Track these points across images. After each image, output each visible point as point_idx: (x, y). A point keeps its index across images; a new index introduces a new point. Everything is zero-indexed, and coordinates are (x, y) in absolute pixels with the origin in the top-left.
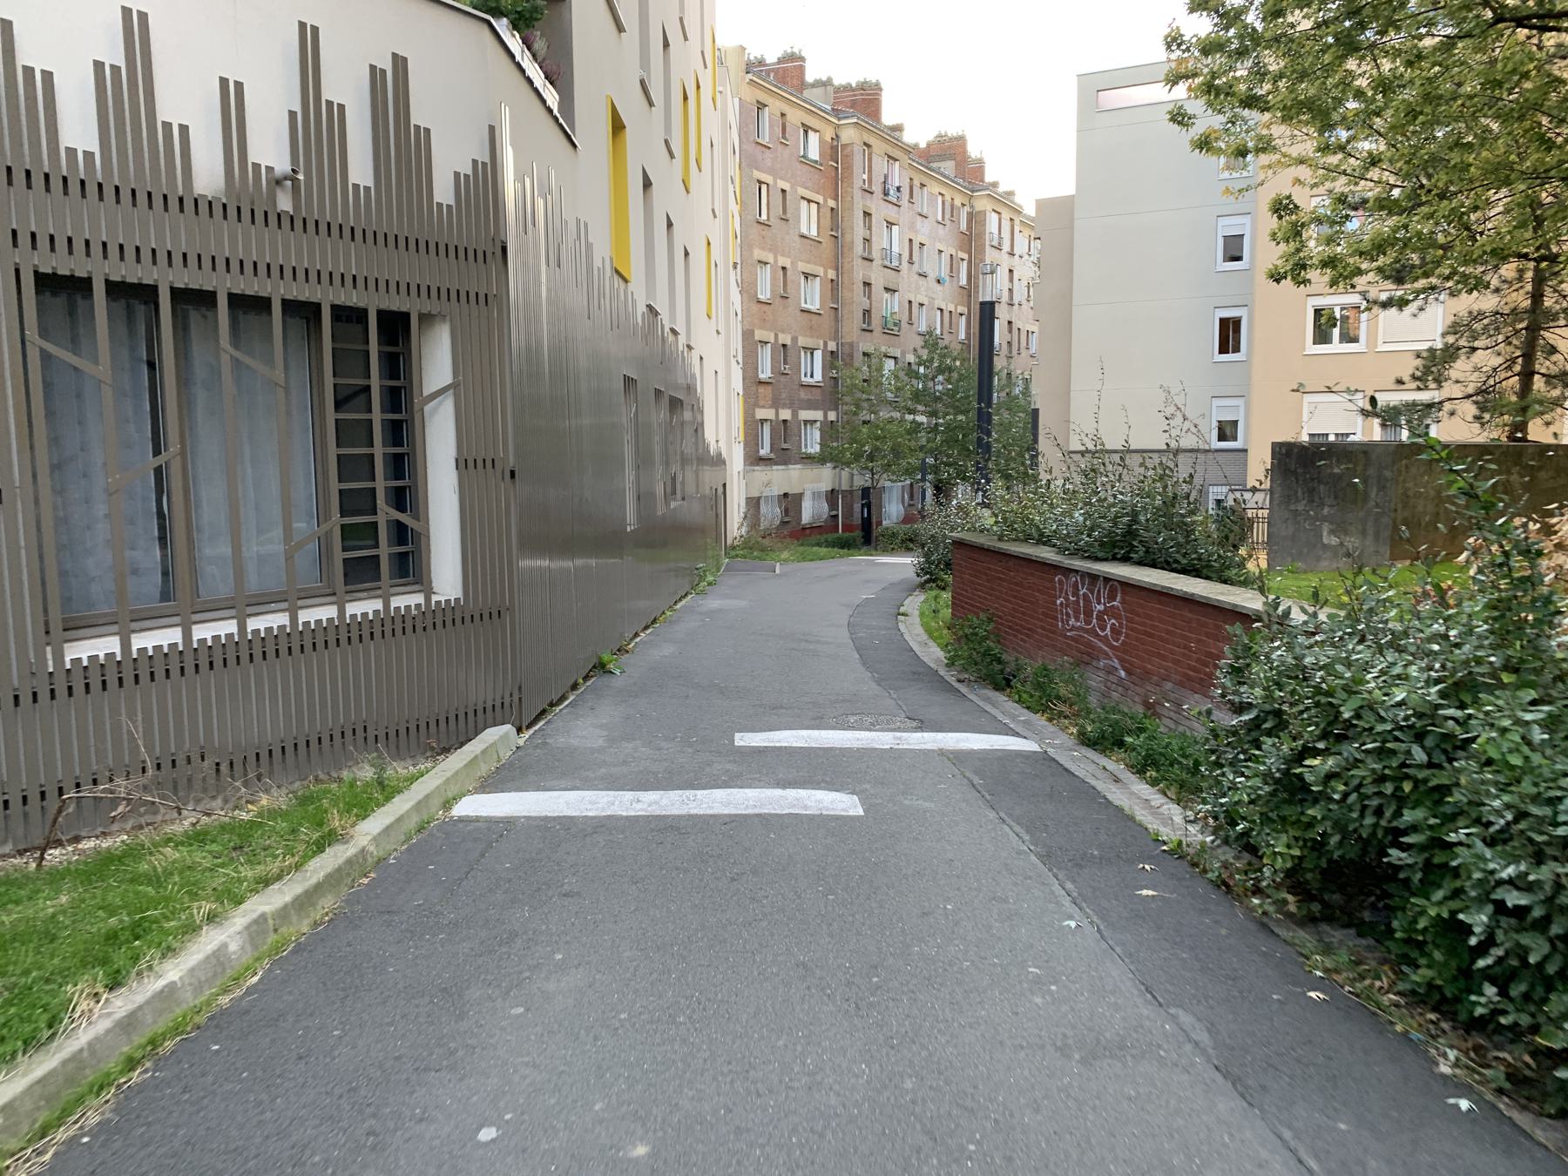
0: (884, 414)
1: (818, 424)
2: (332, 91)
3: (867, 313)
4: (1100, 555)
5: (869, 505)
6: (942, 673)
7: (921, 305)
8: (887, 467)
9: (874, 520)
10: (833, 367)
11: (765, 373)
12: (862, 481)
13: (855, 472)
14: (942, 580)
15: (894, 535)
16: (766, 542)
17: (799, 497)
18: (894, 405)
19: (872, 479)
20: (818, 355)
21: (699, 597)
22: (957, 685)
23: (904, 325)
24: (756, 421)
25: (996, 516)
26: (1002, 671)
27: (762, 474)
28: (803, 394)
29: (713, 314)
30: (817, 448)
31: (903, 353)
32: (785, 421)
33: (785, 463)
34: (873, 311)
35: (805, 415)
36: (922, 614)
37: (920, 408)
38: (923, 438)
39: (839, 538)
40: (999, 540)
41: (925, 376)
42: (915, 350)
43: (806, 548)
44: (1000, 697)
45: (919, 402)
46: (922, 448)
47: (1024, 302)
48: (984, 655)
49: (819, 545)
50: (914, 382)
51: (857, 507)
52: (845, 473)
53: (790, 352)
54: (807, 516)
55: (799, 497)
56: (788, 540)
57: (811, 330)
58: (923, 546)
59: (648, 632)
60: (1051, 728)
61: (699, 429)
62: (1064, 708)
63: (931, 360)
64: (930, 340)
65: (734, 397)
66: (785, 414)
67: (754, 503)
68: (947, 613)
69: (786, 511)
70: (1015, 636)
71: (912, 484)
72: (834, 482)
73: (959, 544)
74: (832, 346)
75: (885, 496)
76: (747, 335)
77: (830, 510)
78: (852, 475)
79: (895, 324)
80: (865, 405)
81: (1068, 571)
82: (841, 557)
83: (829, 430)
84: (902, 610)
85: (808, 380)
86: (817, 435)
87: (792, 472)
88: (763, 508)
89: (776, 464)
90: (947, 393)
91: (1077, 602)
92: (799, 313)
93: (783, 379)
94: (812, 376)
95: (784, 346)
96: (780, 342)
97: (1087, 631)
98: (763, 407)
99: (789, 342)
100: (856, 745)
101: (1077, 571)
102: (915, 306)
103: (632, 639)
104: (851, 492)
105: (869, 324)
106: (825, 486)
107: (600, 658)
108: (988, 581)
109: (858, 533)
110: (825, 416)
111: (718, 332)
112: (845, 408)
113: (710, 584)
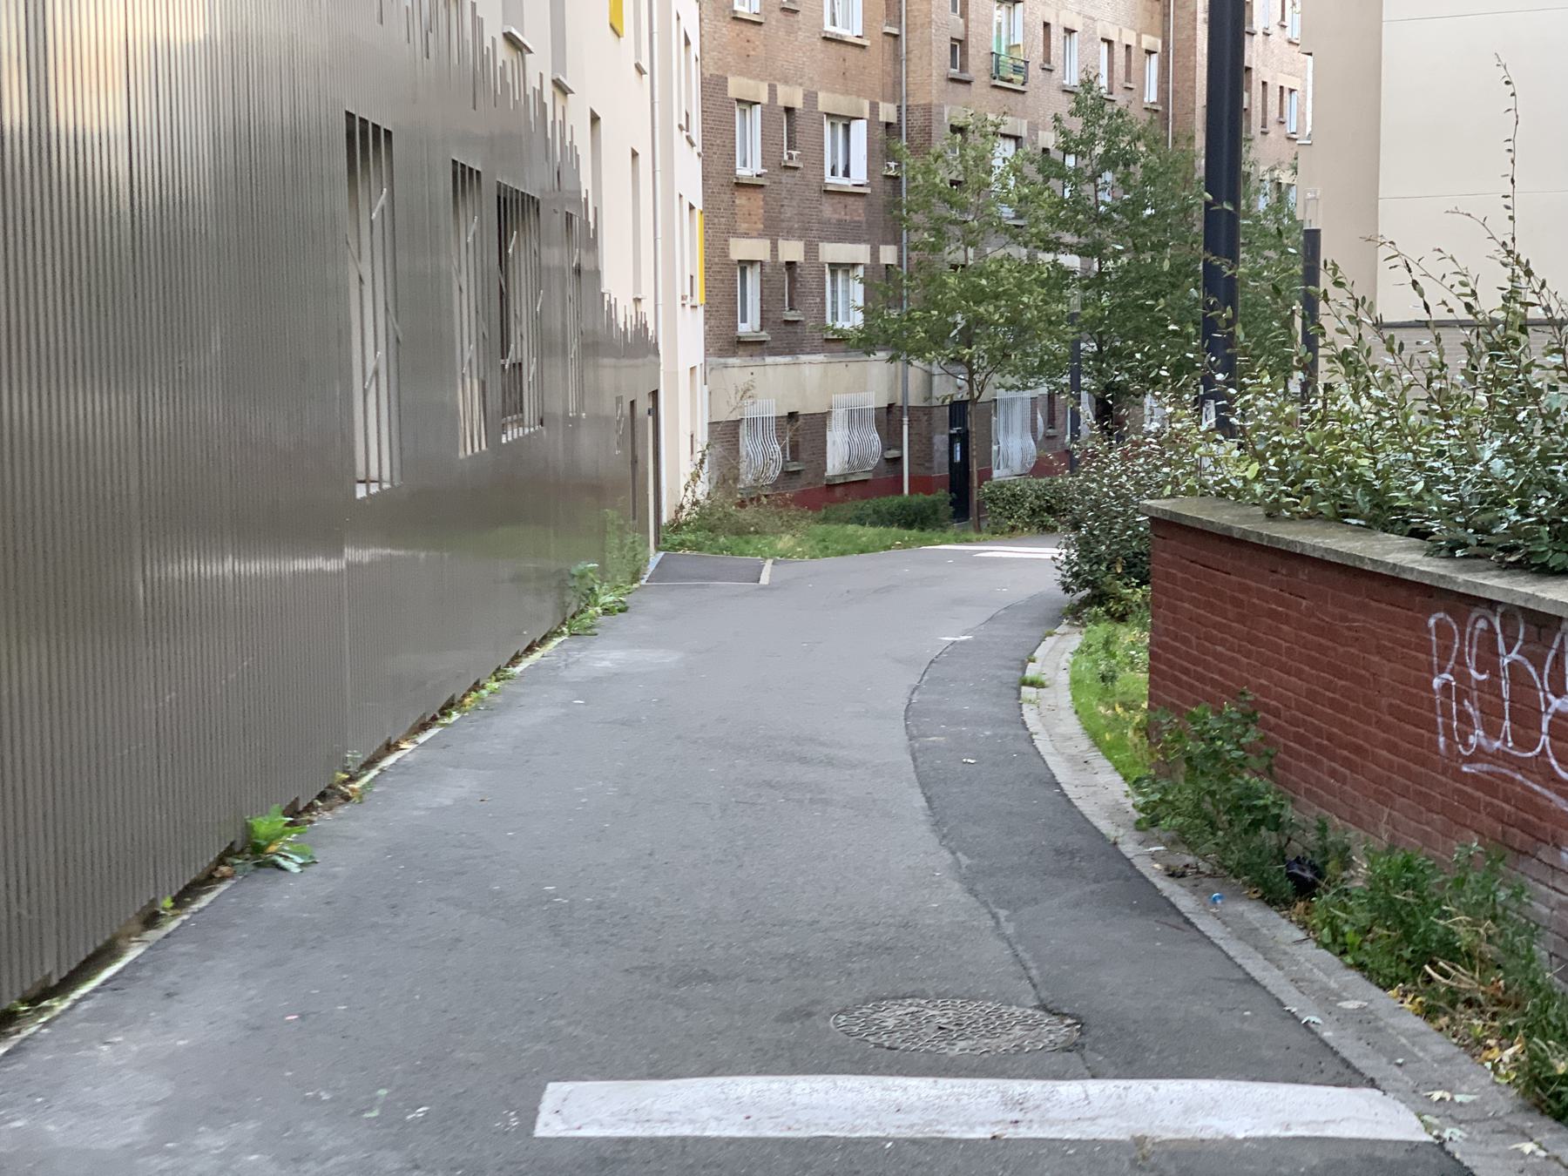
0: (995, 250)
1: (860, 271)
2: (545, 100)
3: (959, 46)
4: (1555, 560)
5: (964, 438)
6: (1129, 848)
7: (1070, 32)
8: (999, 359)
9: (974, 468)
10: (890, 154)
11: (750, 167)
12: (949, 387)
13: (936, 370)
14: (1119, 600)
15: (1016, 499)
16: (747, 515)
17: (819, 422)
18: (1014, 234)
19: (970, 382)
20: (859, 130)
21: (576, 644)
22: (1166, 886)
23: (1034, 70)
24: (729, 265)
25: (1263, 460)
26: (1280, 855)
27: (739, 370)
28: (829, 210)
29: (628, 28)
30: (858, 319)
31: (1034, 128)
32: (791, 265)
33: (792, 350)
34: (972, 40)
35: (833, 252)
36: (1076, 683)
37: (1068, 238)
38: (1074, 296)
39: (903, 507)
40: (1269, 516)
41: (1077, 171)
42: (1057, 119)
43: (833, 527)
44: (1283, 929)
45: (1063, 225)
46: (1072, 318)
47: (1274, 29)
48: (1235, 809)
49: (860, 521)
50: (1055, 183)
51: (940, 441)
52: (917, 369)
53: (800, 123)
54: (836, 461)
55: (819, 422)
56: (793, 511)
57: (845, 80)
58: (1076, 527)
59: (423, 738)
60: (1436, 1045)
61: (585, 276)
62: (1465, 981)
63: (1090, 141)
64: (1088, 101)
65: (680, 215)
66: (792, 250)
67: (726, 434)
68: (1136, 681)
69: (794, 451)
70: (1313, 762)
71: (1051, 397)
72: (892, 389)
73: (1165, 525)
74: (887, 112)
75: (998, 421)
76: (712, 87)
77: (886, 447)
78: (930, 375)
79: (1017, 70)
80: (956, 231)
81: (1464, 603)
82: (906, 545)
83: (882, 284)
84: (1032, 671)
85: (839, 181)
86: (858, 293)
87: (806, 369)
88: (746, 444)
89: (775, 352)
90: (1122, 208)
91: (1493, 686)
92: (819, 44)
93: (785, 177)
94: (847, 174)
95: (789, 111)
96: (781, 102)
97: (1520, 765)
98: (746, 235)
99: (798, 103)
100: (893, 1127)
101: (1492, 604)
102: (1057, 34)
103: (370, 764)
104: (928, 411)
105: (963, 68)
106: (875, 397)
107: (249, 829)
108: (1241, 619)
109: (942, 495)
110: (875, 254)
111: (638, 68)
112: (915, 238)
113: (607, 611)
